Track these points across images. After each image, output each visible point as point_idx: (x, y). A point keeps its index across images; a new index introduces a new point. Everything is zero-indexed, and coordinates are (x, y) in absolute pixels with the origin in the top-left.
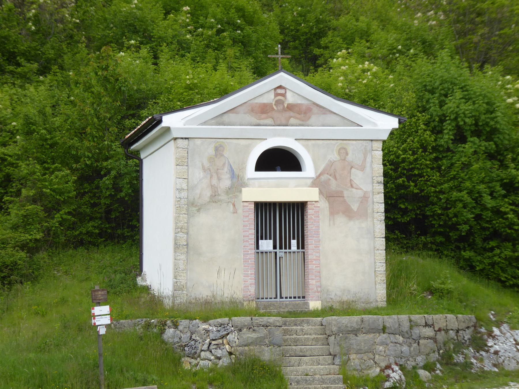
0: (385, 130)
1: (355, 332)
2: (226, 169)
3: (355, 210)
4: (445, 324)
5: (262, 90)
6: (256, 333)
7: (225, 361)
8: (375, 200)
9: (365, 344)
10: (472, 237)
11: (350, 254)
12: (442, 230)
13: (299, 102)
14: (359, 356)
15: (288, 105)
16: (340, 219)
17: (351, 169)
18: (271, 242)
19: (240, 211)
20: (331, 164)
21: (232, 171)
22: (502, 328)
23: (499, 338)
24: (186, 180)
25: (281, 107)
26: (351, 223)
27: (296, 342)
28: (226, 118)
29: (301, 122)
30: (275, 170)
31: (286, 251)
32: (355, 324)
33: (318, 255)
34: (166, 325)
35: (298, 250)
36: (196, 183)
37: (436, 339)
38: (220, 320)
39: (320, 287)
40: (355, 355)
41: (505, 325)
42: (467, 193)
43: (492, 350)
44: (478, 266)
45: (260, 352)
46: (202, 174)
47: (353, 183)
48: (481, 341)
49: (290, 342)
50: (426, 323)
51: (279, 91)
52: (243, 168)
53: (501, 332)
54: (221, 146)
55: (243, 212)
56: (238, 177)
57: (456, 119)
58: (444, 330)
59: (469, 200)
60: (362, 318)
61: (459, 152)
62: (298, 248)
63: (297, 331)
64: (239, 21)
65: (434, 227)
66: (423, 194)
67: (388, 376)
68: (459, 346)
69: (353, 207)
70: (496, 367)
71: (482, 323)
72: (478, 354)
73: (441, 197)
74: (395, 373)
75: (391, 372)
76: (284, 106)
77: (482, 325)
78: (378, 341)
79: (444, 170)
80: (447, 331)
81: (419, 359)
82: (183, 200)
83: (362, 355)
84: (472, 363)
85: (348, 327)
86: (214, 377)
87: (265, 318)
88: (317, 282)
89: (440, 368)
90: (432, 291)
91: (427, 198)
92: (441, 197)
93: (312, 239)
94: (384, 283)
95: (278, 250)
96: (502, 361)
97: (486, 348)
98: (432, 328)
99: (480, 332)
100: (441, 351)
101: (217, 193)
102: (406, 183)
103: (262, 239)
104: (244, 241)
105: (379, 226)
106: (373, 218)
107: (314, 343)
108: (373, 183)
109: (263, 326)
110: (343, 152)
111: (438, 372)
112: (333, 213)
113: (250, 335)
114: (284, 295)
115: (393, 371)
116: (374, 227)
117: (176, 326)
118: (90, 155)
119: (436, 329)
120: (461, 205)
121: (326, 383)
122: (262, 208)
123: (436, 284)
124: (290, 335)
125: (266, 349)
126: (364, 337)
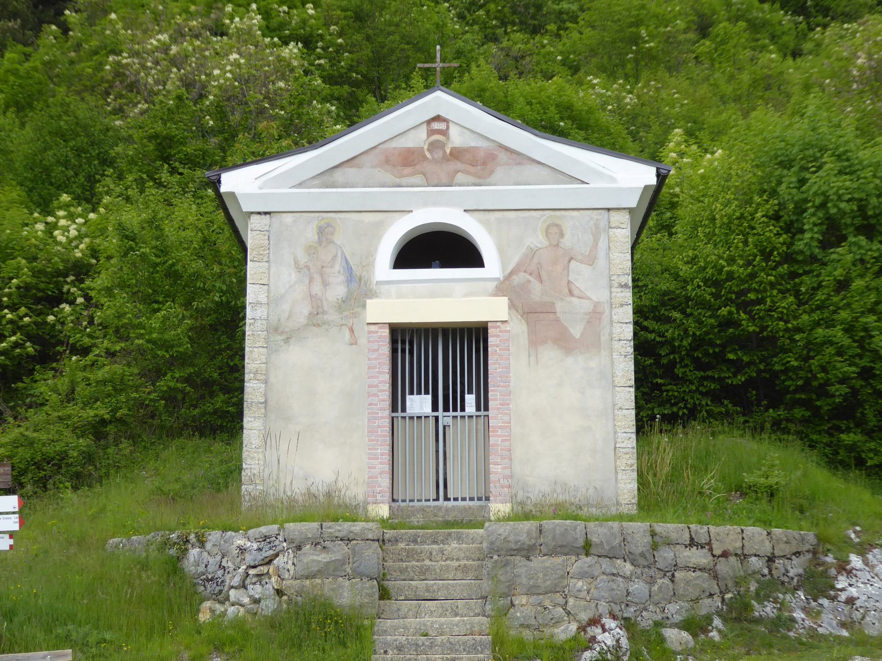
0: (636, 188)
1: (527, 552)
2: (337, 267)
3: (578, 336)
4: (739, 544)
5: (401, 123)
6: (327, 553)
7: (269, 606)
8: (615, 317)
9: (545, 575)
10: (861, 410)
11: (567, 420)
12: (803, 396)
13: (473, 144)
14: (533, 599)
15: (453, 149)
16: (549, 354)
17: (569, 261)
18: (429, 398)
19: (363, 341)
20: (532, 253)
21: (349, 270)
22: (870, 556)
23: (859, 573)
24: (266, 287)
25: (439, 154)
26: (570, 360)
27: (424, 574)
28: (338, 176)
29: (477, 181)
30: (428, 265)
31: (455, 414)
32: (525, 535)
33: (506, 418)
34: (188, 541)
35: (478, 413)
36: (283, 292)
37: (715, 572)
38: (264, 530)
39: (511, 477)
40: (525, 596)
41: (876, 551)
42: (843, 329)
43: (843, 597)
44: (871, 459)
45: (333, 590)
46: (293, 275)
47: (573, 287)
48: (824, 580)
49: (412, 574)
50: (692, 539)
51: (436, 126)
52: (368, 262)
53: (866, 562)
54: (329, 225)
55: (369, 342)
56: (360, 280)
57: (823, 205)
58: (736, 555)
59: (847, 341)
60: (541, 526)
61: (832, 261)
62: (478, 409)
63: (431, 554)
64: (562, 124)
65: (789, 392)
66: (765, 334)
67: (593, 639)
68: (770, 587)
69: (572, 331)
70: (847, 629)
71: (829, 547)
72: (813, 604)
73: (797, 337)
74: (607, 634)
75: (599, 630)
76: (445, 152)
77: (828, 550)
78: (573, 570)
79: (806, 293)
80: (743, 557)
81: (672, 608)
82: (260, 322)
83: (541, 597)
84: (793, 620)
85: (509, 542)
86: (230, 638)
87: (347, 525)
88: (507, 468)
89: (721, 626)
90: (743, 490)
91: (773, 339)
92: (797, 337)
93: (496, 391)
94: (633, 470)
95: (440, 413)
96: (859, 616)
97: (832, 593)
98: (705, 551)
99: (824, 564)
100: (728, 596)
101: (320, 310)
102: (736, 316)
103: (412, 393)
104: (370, 395)
105: (622, 365)
106: (612, 350)
107: (459, 575)
108: (611, 287)
109: (341, 540)
110: (554, 232)
111: (714, 634)
112: (535, 342)
113: (315, 558)
114: (451, 495)
115: (604, 630)
116: (613, 368)
117: (202, 543)
118: (224, 288)
119: (717, 552)
120: (831, 350)
121: (456, 651)
122: (404, 338)
123: (749, 478)
124: (418, 561)
125: (347, 583)
126: (543, 562)
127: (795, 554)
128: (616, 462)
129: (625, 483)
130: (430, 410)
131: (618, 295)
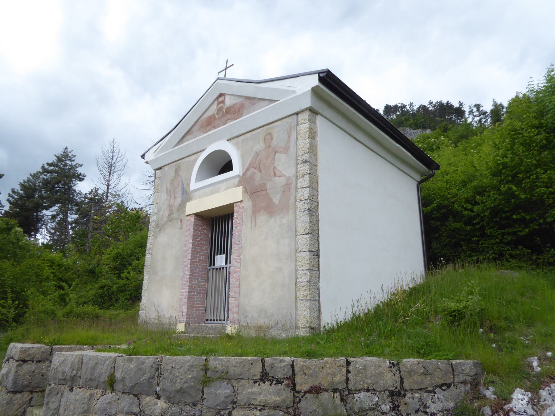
0: (309, 91)
2: (180, 188)
16: (262, 217)
20: (257, 154)
62: (226, 263)
69: (274, 200)
103: (217, 255)
116: (296, 221)
127: (440, 386)
128: (296, 294)
129: (302, 311)
130: (224, 264)
131: (301, 169)
